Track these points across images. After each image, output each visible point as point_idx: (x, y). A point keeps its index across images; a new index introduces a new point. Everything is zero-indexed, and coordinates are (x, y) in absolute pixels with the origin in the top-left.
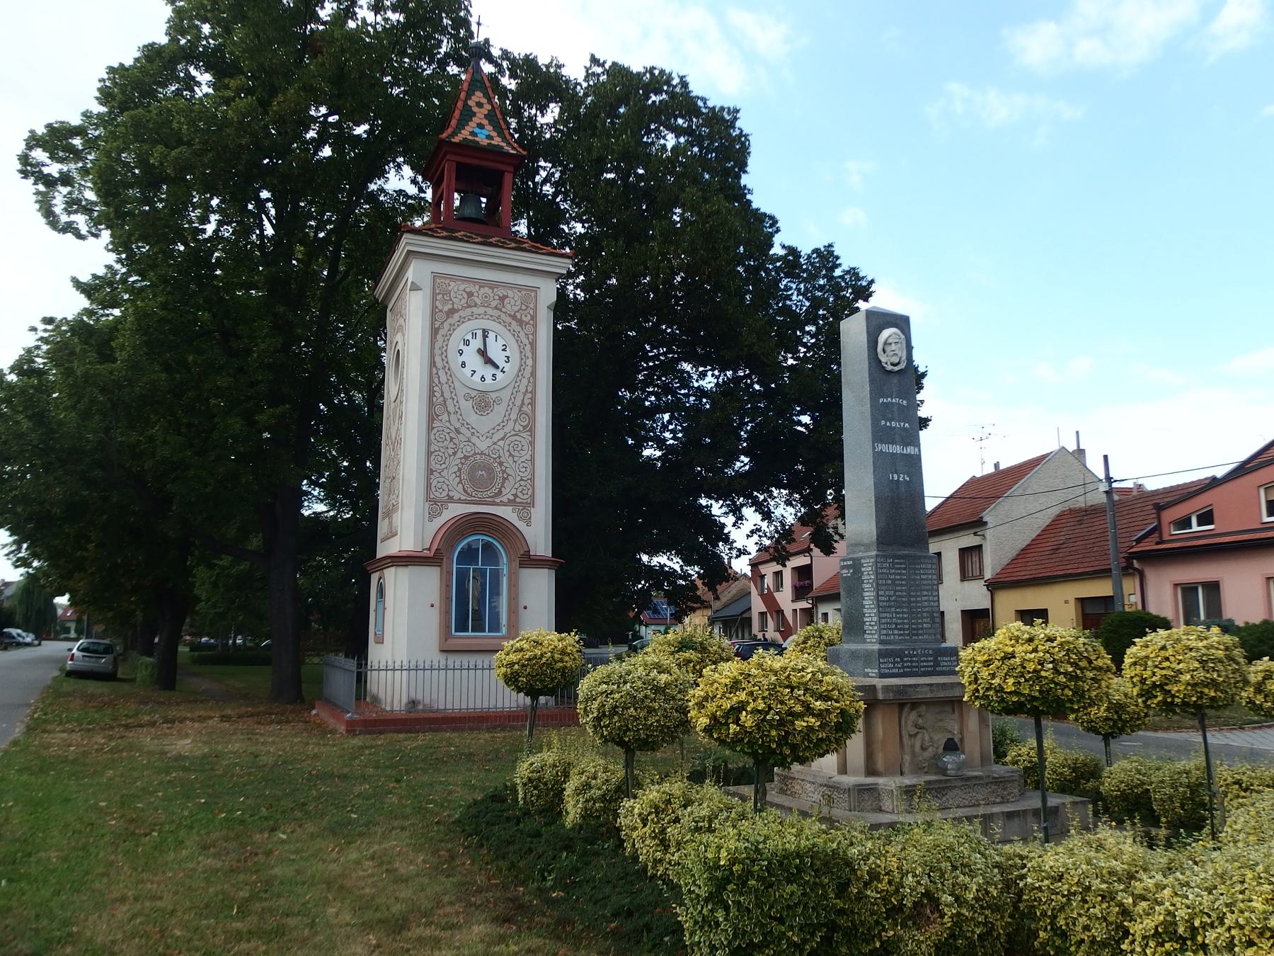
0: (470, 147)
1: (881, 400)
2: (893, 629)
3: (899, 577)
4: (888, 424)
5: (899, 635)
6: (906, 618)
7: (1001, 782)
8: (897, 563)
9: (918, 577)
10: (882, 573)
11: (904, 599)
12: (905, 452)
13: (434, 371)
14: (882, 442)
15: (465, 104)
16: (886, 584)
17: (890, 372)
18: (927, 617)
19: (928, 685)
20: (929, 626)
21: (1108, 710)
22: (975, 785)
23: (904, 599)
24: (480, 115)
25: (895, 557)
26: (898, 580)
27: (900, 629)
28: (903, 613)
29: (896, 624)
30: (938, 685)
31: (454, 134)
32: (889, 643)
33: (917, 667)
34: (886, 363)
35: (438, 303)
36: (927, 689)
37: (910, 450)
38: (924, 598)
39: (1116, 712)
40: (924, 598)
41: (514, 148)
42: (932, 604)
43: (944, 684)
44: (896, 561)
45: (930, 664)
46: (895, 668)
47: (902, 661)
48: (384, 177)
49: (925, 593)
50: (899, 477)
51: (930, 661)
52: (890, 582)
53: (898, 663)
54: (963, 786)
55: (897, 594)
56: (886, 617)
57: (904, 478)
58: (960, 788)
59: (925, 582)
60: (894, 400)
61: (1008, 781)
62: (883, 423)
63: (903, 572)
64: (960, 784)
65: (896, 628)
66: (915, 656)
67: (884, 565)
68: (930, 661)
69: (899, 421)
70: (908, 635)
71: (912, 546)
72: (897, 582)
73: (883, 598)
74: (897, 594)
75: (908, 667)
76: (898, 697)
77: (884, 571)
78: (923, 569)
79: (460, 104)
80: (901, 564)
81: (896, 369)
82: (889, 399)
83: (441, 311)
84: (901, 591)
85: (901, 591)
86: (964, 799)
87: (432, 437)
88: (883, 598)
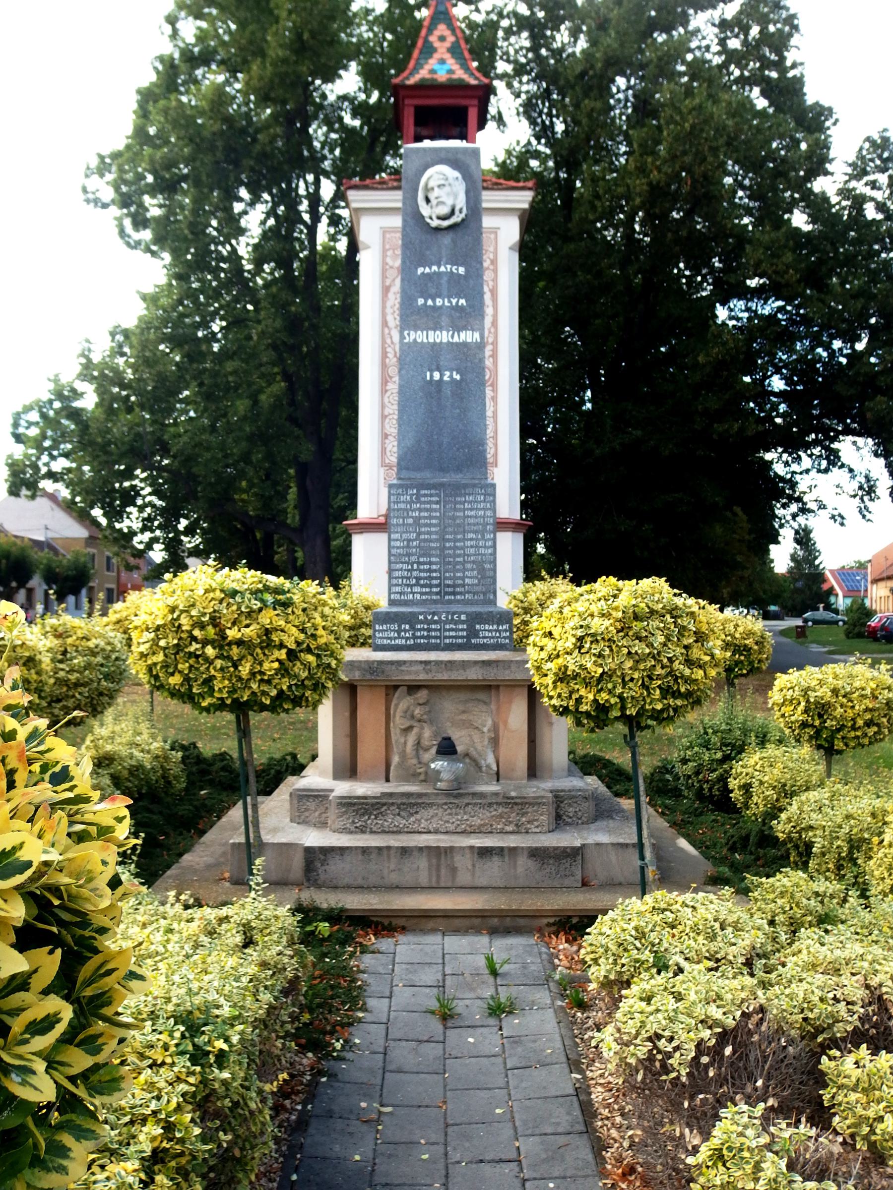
0: (428, 87)
1: (420, 270)
2: (412, 586)
3: (426, 514)
4: (430, 302)
5: (422, 594)
6: (435, 571)
7: (516, 804)
8: (425, 495)
9: (461, 514)
10: (398, 510)
11: (432, 545)
12: (456, 339)
13: (386, 331)
14: (416, 328)
15: (426, 41)
16: (404, 524)
17: (438, 229)
18: (473, 570)
19: (421, 662)
20: (476, 581)
21: (806, 711)
22: (467, 804)
23: (432, 545)
24: (442, 49)
25: (421, 486)
26: (425, 518)
27: (422, 586)
28: (431, 563)
29: (418, 579)
30: (438, 663)
31: (407, 78)
32: (406, 603)
33: (439, 637)
34: (431, 218)
35: (389, 260)
36: (420, 667)
37: (468, 336)
38: (469, 543)
39: (820, 716)
40: (469, 543)
41: (476, 78)
42: (482, 551)
43: (450, 662)
44: (422, 492)
45: (460, 634)
46: (399, 637)
47: (412, 628)
48: (228, 120)
49: (471, 536)
50: (442, 375)
51: (462, 630)
52: (410, 521)
53: (405, 631)
54: (446, 804)
55: (422, 537)
56: (401, 570)
57: (451, 376)
58: (439, 806)
59: (472, 521)
60: (443, 269)
61: (530, 804)
62: (421, 301)
63: (434, 506)
64: (399, 801)
65: (417, 584)
66: (436, 622)
67: (402, 498)
68: (462, 630)
69: (449, 297)
70: (437, 594)
71: (459, 469)
72: (422, 521)
73: (398, 544)
74: (422, 537)
75: (422, 637)
76: (368, 677)
77: (402, 506)
78: (470, 502)
79: (420, 43)
80: (431, 495)
81: (446, 223)
82: (435, 268)
83: (391, 267)
84: (429, 533)
85: (429, 533)
86: (448, 822)
87: (386, 400)
88: (398, 544)
